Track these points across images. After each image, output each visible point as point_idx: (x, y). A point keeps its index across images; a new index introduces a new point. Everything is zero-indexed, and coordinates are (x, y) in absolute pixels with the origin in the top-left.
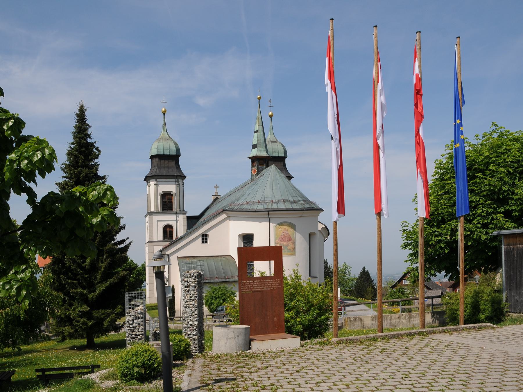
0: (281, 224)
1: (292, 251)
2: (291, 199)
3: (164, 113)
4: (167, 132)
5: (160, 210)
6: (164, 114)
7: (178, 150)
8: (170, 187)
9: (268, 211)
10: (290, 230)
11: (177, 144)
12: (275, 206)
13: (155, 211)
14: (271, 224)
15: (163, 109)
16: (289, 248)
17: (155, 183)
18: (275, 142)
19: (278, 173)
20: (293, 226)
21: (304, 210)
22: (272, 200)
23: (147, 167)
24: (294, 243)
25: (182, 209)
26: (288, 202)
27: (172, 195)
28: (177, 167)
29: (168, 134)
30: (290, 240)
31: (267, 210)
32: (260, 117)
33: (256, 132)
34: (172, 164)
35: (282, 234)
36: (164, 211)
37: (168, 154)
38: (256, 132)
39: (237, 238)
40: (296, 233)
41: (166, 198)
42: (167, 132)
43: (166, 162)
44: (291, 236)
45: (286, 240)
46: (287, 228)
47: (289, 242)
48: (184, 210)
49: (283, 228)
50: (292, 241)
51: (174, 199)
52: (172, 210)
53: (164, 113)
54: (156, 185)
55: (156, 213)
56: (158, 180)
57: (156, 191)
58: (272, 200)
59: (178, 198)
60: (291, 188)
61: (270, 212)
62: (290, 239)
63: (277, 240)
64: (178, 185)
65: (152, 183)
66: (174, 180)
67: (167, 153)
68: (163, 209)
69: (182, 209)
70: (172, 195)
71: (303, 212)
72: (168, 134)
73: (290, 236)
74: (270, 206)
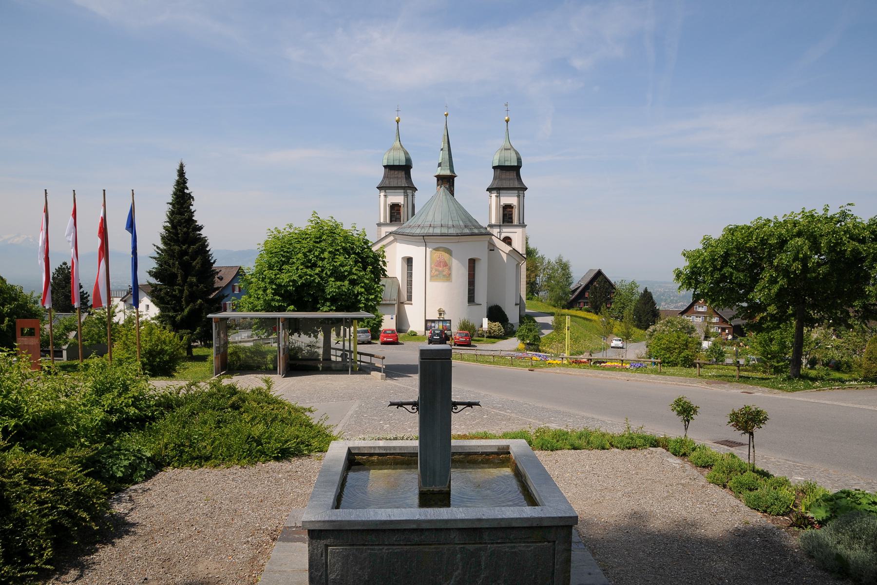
0: (437, 249)
1: (447, 277)
2: (450, 223)
3: (507, 121)
4: (400, 141)
5: (388, 221)
6: (507, 122)
7: (519, 160)
8: (510, 199)
9: (423, 236)
10: (446, 256)
11: (519, 154)
12: (431, 231)
13: (496, 224)
14: (427, 248)
15: (397, 118)
16: (444, 273)
17: (385, 194)
18: (509, 149)
19: (446, 195)
20: (449, 252)
21: (459, 236)
22: (453, 225)
23: (489, 177)
24: (450, 269)
25: (521, 222)
26: (445, 226)
27: (512, 207)
28: (406, 178)
29: (400, 143)
30: (446, 266)
31: (423, 235)
32: (446, 134)
33: (442, 150)
34: (513, 174)
35: (438, 259)
36: (393, 223)
37: (398, 164)
38: (442, 150)
39: (400, 260)
40: (453, 259)
41: (395, 209)
42: (400, 141)
43: (396, 172)
44: (447, 262)
45: (442, 265)
46: (443, 253)
47: (444, 268)
48: (524, 223)
49: (438, 253)
50: (447, 267)
51: (402, 209)
52: (400, 221)
53: (507, 121)
54: (385, 196)
55: (385, 224)
56: (387, 191)
57: (385, 202)
58: (453, 225)
59: (406, 209)
60: (454, 212)
61: (425, 237)
62: (446, 265)
63: (432, 266)
64: (406, 196)
65: (494, 195)
66: (403, 191)
67: (397, 163)
68: (391, 221)
69: (521, 222)
70: (512, 207)
71: (458, 237)
72: (400, 143)
73: (445, 261)
74: (425, 231)
